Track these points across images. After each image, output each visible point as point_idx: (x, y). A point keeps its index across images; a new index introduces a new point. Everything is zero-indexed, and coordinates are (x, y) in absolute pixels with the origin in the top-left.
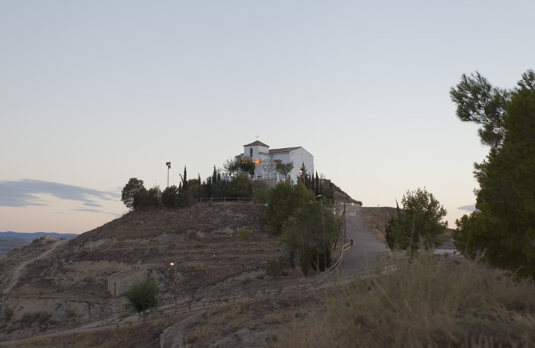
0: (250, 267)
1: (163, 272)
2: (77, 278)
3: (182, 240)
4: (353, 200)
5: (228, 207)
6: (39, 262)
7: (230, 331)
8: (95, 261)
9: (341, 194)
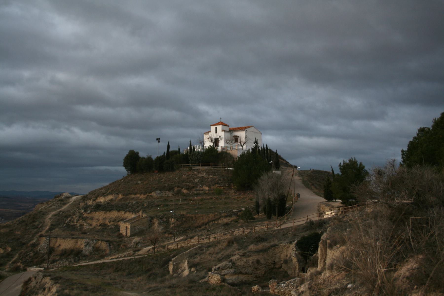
0: (225, 214)
1: (161, 219)
2: (94, 224)
3: (171, 195)
4: (291, 165)
5: (204, 171)
6: (63, 212)
7: (221, 260)
8: (108, 211)
9: (282, 161)
